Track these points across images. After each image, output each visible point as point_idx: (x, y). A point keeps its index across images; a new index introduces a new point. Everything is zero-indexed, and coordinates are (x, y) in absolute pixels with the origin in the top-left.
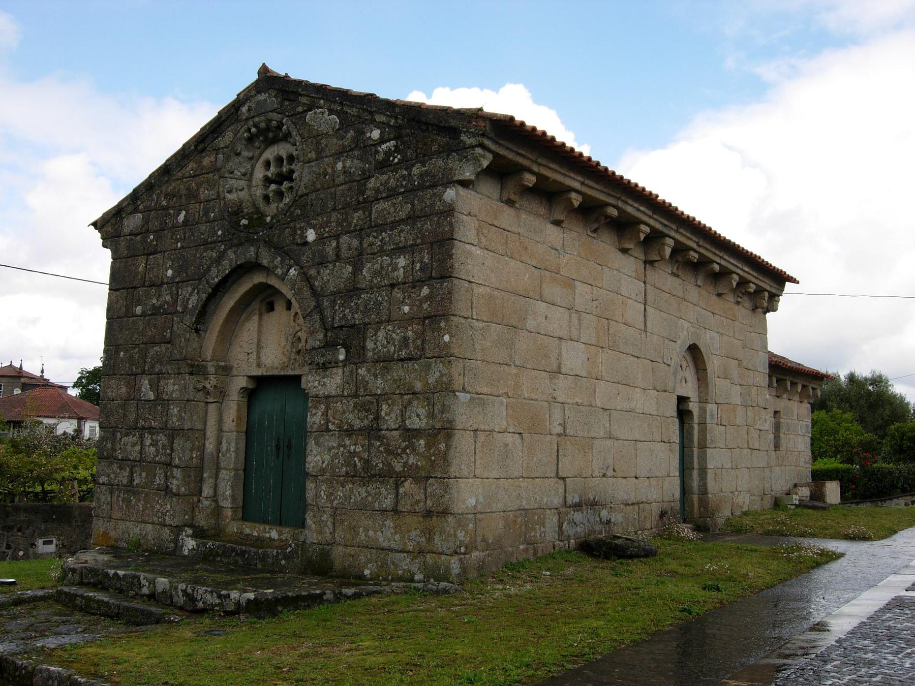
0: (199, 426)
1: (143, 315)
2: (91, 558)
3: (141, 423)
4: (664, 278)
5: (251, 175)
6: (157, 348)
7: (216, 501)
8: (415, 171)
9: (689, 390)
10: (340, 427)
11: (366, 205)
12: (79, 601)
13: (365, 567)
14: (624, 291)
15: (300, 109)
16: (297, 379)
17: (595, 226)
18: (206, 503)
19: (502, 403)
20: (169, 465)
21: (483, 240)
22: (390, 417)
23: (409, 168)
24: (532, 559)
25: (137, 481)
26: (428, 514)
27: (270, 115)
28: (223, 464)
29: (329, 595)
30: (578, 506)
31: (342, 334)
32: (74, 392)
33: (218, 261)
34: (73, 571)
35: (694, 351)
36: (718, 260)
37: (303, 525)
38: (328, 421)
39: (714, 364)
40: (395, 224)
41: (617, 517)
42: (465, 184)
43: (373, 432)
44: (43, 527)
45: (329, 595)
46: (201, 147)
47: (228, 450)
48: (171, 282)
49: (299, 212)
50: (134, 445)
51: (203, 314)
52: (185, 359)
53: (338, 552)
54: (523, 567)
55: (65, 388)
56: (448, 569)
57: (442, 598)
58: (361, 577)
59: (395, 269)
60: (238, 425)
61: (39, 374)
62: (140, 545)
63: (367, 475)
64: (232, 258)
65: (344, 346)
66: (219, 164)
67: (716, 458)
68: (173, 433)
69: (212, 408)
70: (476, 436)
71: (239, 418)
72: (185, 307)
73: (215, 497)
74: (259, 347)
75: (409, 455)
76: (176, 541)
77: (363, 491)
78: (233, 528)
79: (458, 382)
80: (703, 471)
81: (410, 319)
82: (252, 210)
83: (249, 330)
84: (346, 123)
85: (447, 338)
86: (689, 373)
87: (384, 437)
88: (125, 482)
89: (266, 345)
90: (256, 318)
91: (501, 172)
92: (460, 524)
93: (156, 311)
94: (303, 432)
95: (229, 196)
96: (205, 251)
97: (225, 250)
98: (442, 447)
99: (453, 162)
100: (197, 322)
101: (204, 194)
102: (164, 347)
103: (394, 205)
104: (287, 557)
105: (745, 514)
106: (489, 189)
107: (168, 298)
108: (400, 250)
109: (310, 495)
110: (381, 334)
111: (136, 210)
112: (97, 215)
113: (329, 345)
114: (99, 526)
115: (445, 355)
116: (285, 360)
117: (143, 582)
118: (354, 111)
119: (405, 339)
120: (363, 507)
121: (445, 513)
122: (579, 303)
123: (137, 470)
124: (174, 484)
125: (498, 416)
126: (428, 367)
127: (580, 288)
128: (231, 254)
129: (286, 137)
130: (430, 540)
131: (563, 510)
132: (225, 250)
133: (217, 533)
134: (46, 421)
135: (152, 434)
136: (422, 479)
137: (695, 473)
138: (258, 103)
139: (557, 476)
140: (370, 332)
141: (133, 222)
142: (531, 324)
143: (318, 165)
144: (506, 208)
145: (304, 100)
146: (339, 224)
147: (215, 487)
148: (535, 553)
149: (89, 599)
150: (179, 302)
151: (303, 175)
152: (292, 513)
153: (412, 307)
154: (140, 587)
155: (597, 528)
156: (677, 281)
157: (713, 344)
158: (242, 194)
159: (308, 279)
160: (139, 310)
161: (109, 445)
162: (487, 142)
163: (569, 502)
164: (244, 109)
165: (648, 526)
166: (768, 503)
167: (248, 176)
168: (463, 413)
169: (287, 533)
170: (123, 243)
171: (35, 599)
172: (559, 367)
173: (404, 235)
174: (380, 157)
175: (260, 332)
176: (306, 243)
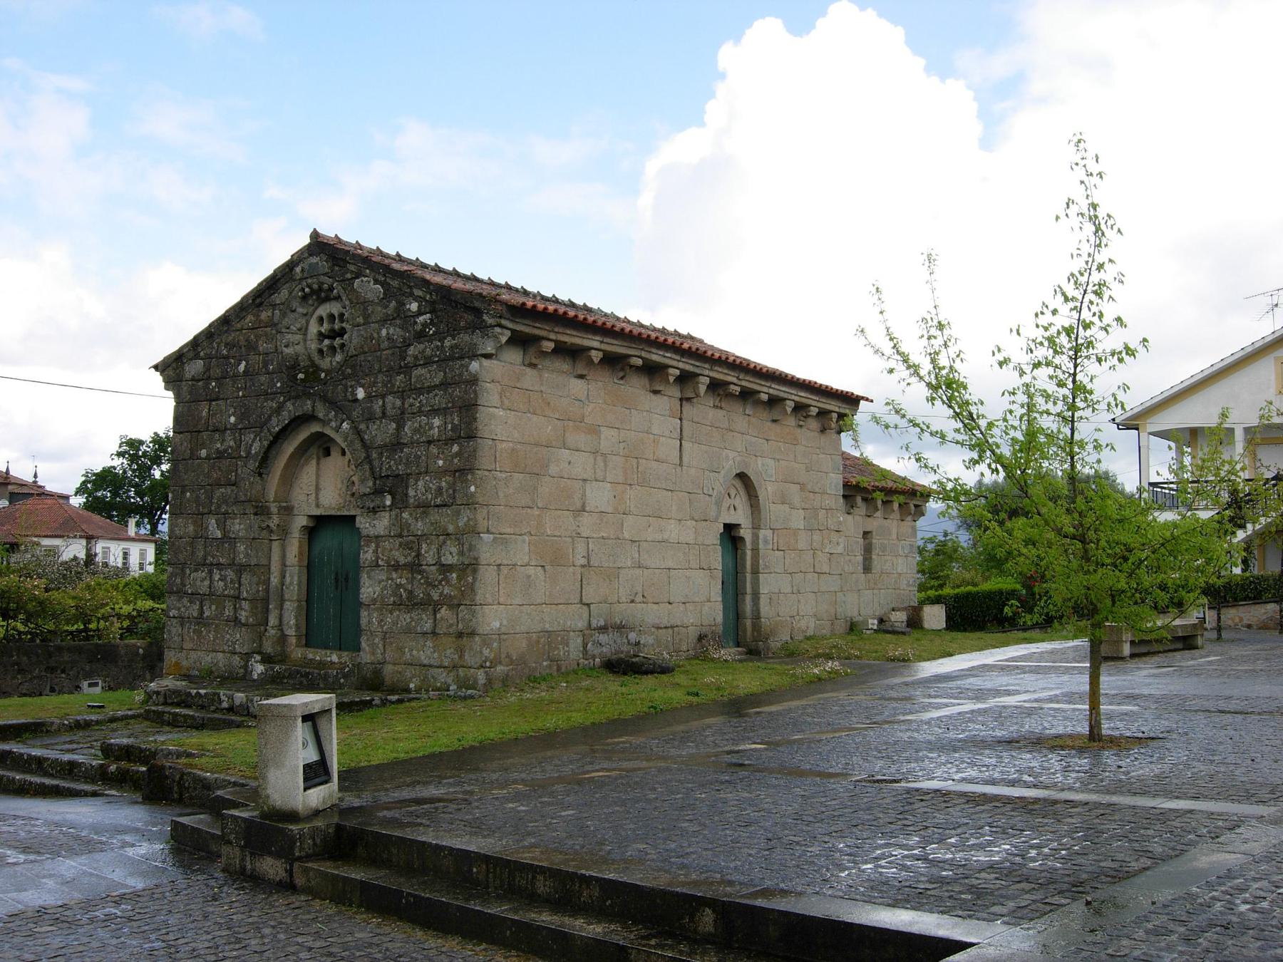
0: (264, 562)
1: (208, 458)
2: (169, 683)
3: (210, 559)
4: (705, 411)
5: (307, 329)
6: (223, 490)
7: (282, 630)
8: (447, 343)
9: (741, 517)
10: (388, 562)
11: (407, 369)
12: (166, 717)
13: (411, 681)
14: (655, 430)
15: (349, 276)
16: (354, 517)
17: (621, 374)
18: (273, 632)
19: (524, 541)
20: (237, 598)
21: (506, 402)
22: (429, 555)
23: (442, 340)
24: (555, 674)
25: (207, 613)
26: (460, 635)
27: (323, 278)
28: (286, 597)
29: (377, 701)
30: (603, 629)
31: (389, 482)
32: (77, 501)
33: (278, 410)
34: (158, 693)
35: (742, 477)
36: (765, 390)
37: (359, 649)
38: (378, 558)
39: (766, 491)
40: (430, 389)
41: (647, 639)
42: (488, 356)
43: (415, 567)
44: (87, 668)
45: (377, 701)
46: (258, 301)
47: (291, 583)
48: (234, 428)
49: (349, 371)
50: (203, 580)
51: (265, 460)
52: (250, 501)
53: (388, 669)
54: (544, 680)
55: (67, 498)
56: (476, 681)
57: (469, 701)
58: (408, 691)
59: (431, 428)
60: (300, 560)
61: (31, 480)
62: (212, 672)
63: (411, 603)
64: (290, 410)
65: (390, 493)
66: (276, 320)
67: (768, 584)
68: (241, 569)
69: (276, 545)
70: (499, 570)
71: (301, 553)
72: (249, 453)
73: (280, 626)
74: (318, 489)
75: (440, 587)
76: (246, 667)
77: (407, 617)
78: (297, 653)
79: (482, 524)
80: (756, 596)
81: (444, 472)
82: (308, 363)
83: (308, 474)
84: (388, 294)
85: (473, 489)
86: (741, 501)
87: (424, 571)
88: (195, 614)
89: (324, 487)
90: (314, 462)
91: (520, 341)
92: (486, 643)
93: (220, 455)
94: (358, 568)
95: (286, 350)
96: (266, 400)
97: (285, 402)
98: (470, 579)
99: (477, 338)
100: (260, 467)
101: (263, 346)
102: (229, 489)
103: (430, 372)
104: (345, 676)
105: (808, 638)
106: (514, 356)
107: (232, 443)
108: (435, 412)
109: (364, 621)
110: (421, 483)
111: (197, 357)
112: (159, 358)
113: (378, 492)
114: (170, 657)
115: (471, 503)
116: (341, 501)
117: (223, 698)
118: (395, 283)
119: (440, 489)
120: (408, 631)
121: (473, 634)
122: (605, 446)
123: (207, 603)
124: (243, 615)
125: (521, 552)
126: (458, 513)
127: (605, 432)
128: (289, 405)
129: (338, 298)
130: (461, 657)
131: (587, 632)
132: (285, 402)
133: (283, 658)
134: (46, 542)
135: (221, 570)
136: (455, 606)
137: (748, 598)
138: (310, 265)
139: (581, 602)
140: (412, 481)
141: (194, 368)
142: (553, 469)
143: (365, 330)
144: (528, 370)
145: (352, 268)
146: (385, 385)
147: (281, 618)
148: (559, 669)
149: (176, 715)
150: (243, 448)
151: (353, 338)
152: (348, 638)
153: (445, 461)
154: (220, 702)
155: (625, 648)
156: (721, 413)
157: (766, 471)
158: (299, 349)
159: (358, 433)
160: (204, 453)
161: (178, 581)
162: (503, 322)
163: (594, 625)
164: (298, 269)
165: (684, 648)
166: (841, 627)
167: (304, 330)
168: (486, 551)
169: (346, 657)
170: (185, 388)
171: (126, 717)
172: (584, 506)
173: (438, 399)
174: (418, 328)
175: (318, 476)
176: (356, 400)
